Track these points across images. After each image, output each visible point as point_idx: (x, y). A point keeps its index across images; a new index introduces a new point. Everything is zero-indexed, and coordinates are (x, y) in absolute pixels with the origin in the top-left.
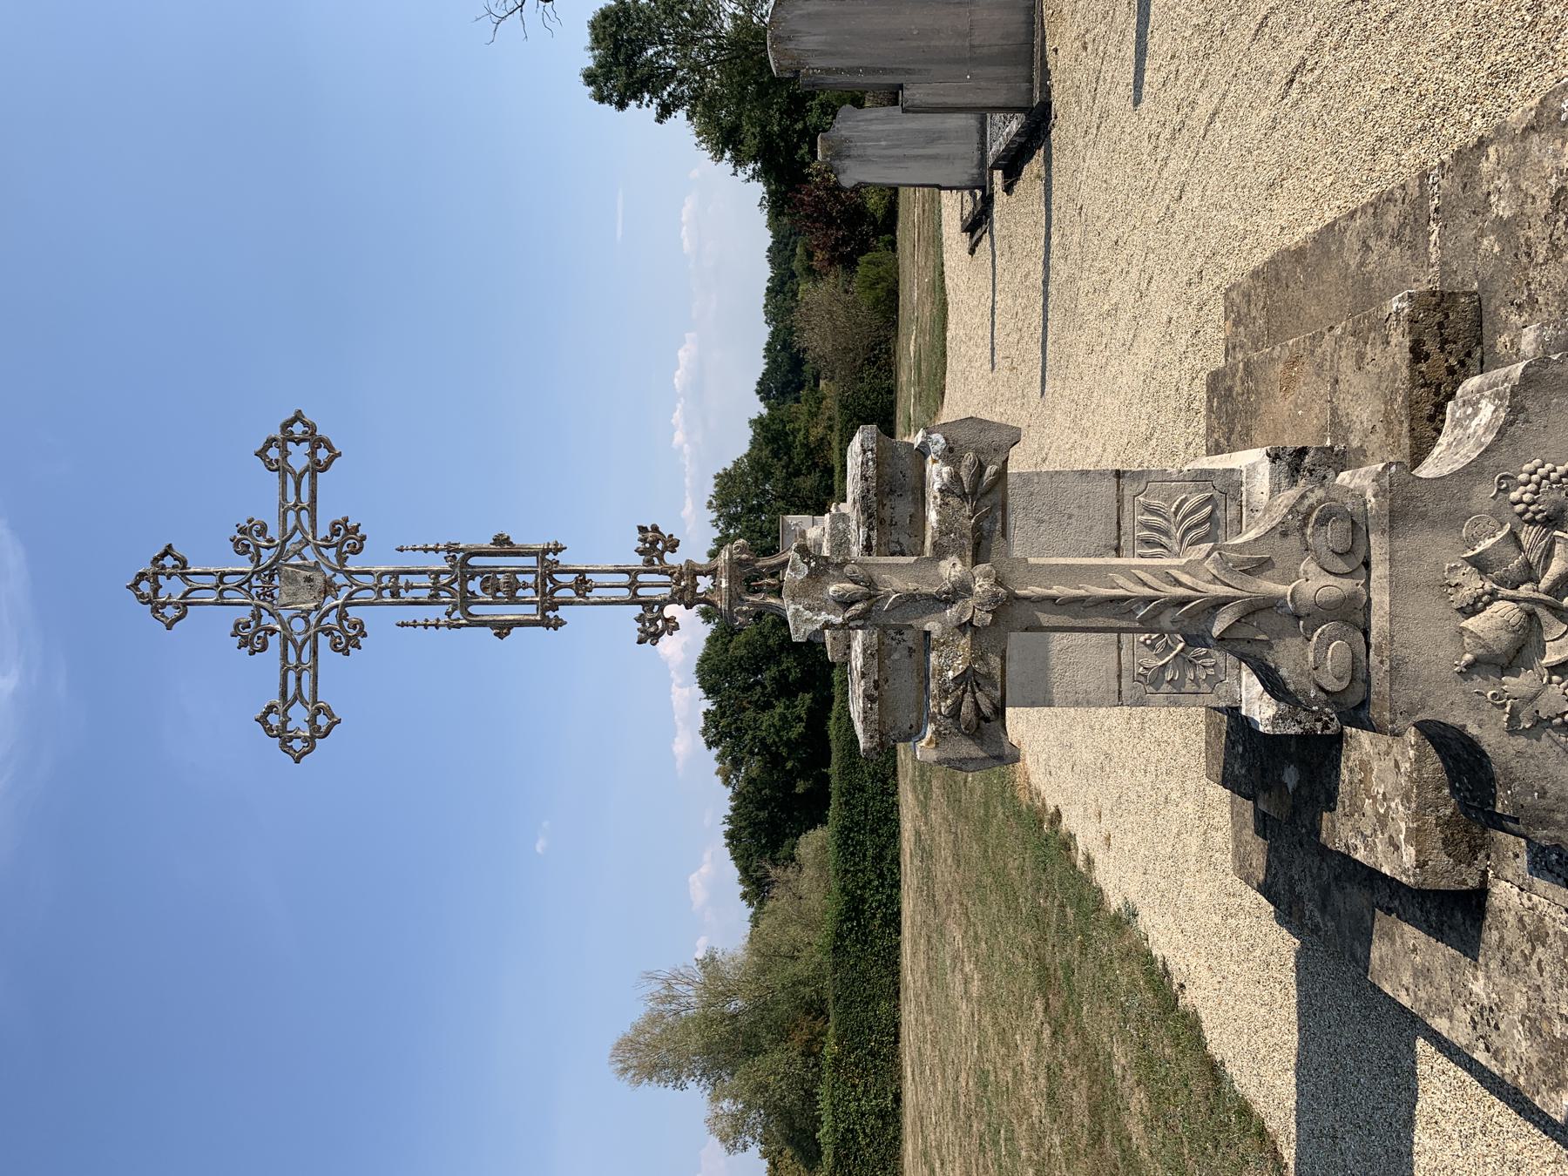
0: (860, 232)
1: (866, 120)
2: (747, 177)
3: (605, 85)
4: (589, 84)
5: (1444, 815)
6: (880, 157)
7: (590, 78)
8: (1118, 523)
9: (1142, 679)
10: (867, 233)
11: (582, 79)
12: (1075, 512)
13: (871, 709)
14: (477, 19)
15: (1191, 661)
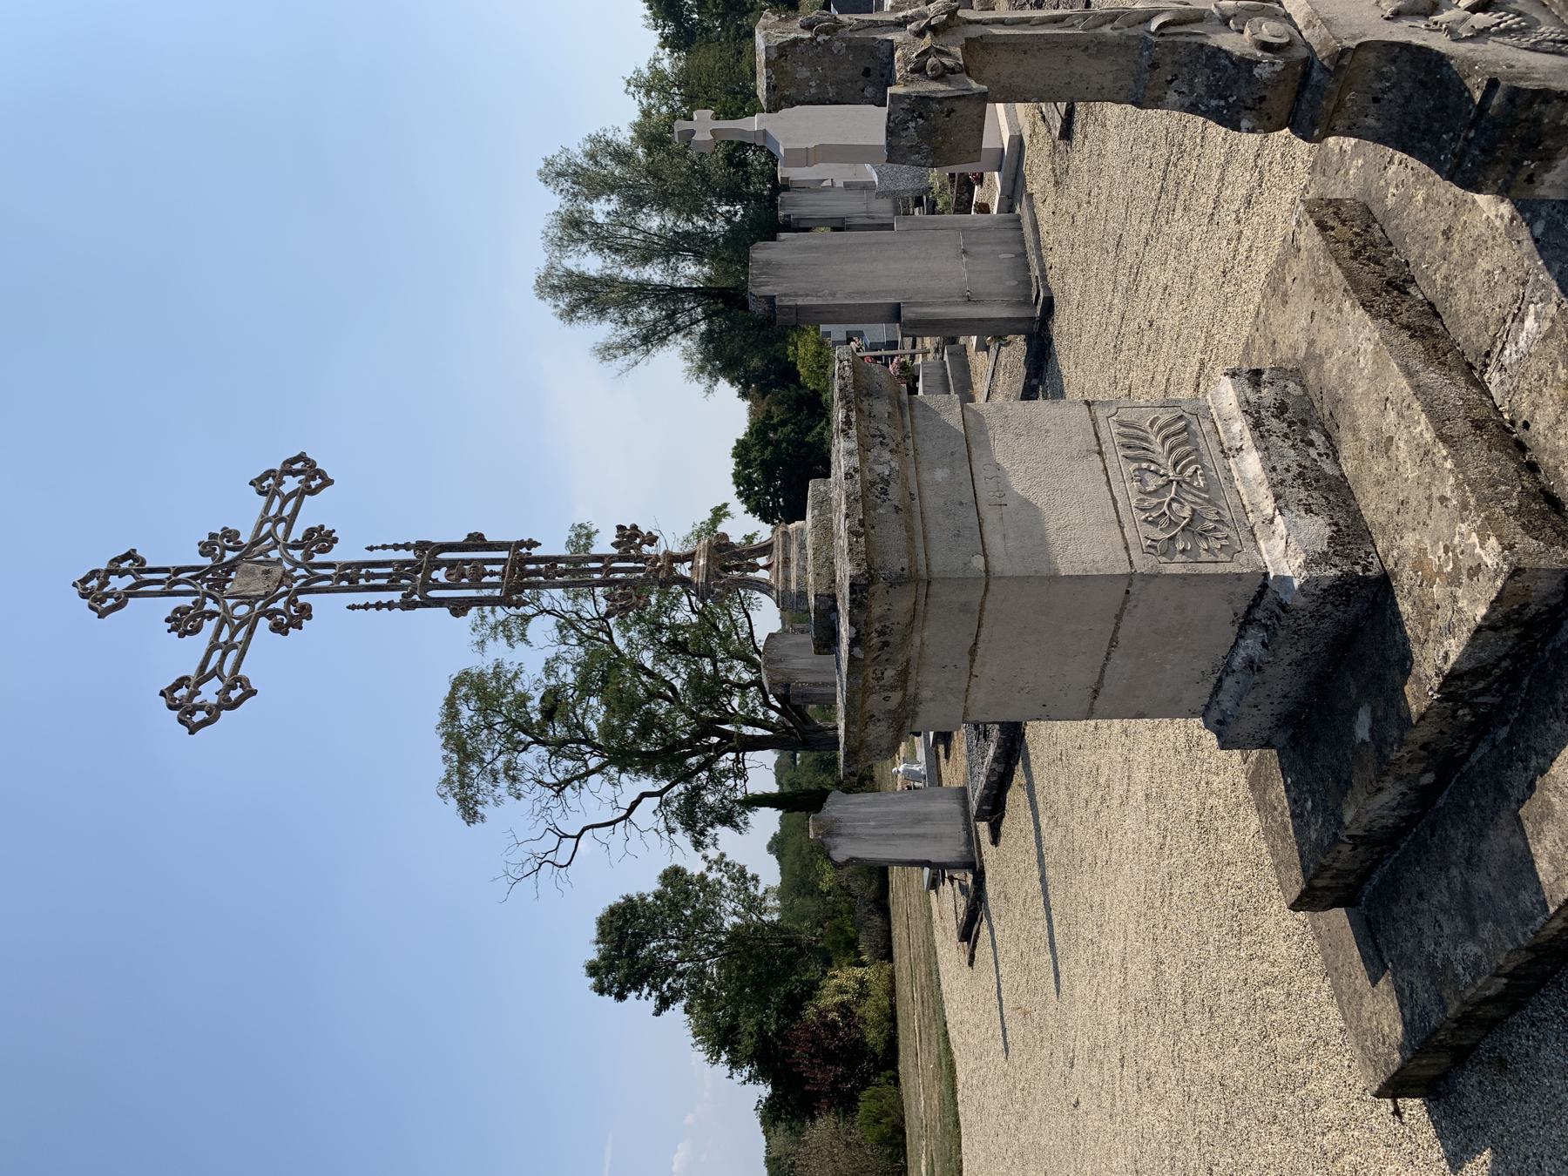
0: (860, 1070)
1: (855, 804)
2: (743, 1079)
3: (606, 977)
4: (591, 975)
6: (870, 835)
7: (593, 970)
8: (1096, 434)
9: (1152, 551)
10: (868, 1071)
11: (584, 970)
12: (1053, 428)
13: (857, 542)
14: (495, 879)
15: (1201, 535)
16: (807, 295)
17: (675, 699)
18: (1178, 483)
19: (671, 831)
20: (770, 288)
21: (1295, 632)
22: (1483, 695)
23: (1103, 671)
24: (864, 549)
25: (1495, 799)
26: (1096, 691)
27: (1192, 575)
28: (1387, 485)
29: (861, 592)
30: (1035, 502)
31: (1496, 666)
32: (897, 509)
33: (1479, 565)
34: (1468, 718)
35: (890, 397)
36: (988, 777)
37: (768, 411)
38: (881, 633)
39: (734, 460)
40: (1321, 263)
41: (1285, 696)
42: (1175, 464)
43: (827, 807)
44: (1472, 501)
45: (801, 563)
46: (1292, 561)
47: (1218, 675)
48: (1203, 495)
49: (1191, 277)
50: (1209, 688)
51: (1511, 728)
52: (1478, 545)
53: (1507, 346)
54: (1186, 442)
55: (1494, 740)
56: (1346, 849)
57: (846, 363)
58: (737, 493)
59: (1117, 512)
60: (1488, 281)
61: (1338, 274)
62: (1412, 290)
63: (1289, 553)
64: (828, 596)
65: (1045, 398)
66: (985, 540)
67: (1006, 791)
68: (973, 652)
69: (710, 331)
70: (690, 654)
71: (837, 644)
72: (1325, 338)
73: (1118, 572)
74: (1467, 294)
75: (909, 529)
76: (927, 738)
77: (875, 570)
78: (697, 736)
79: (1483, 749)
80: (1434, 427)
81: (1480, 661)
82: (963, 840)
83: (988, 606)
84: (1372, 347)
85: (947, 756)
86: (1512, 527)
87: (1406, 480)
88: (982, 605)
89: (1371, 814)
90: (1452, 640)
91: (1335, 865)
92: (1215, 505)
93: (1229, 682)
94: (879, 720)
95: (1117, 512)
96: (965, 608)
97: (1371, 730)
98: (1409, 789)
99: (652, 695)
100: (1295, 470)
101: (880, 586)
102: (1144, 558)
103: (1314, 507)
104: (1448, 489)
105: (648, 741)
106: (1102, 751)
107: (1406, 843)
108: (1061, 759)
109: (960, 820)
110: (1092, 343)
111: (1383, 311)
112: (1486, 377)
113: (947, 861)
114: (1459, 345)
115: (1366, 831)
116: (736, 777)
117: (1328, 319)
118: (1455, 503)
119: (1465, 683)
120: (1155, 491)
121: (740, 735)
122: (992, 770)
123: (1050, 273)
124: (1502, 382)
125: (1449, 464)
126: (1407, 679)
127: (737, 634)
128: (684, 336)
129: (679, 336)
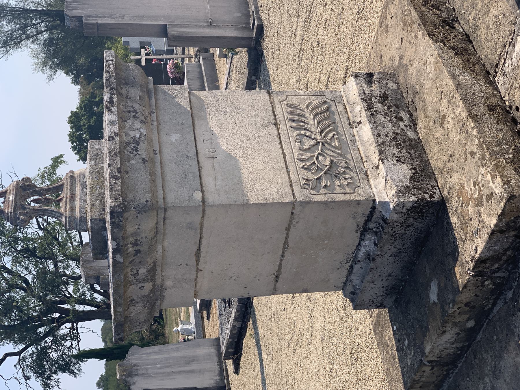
1: (147, 353)
5: (509, 158)
6: (157, 374)
8: (274, 112)
9: (307, 187)
12: (247, 108)
13: (115, 183)
15: (336, 176)
16: (105, 17)
17: (27, 287)
18: (323, 143)
19: (27, 378)
20: (79, 11)
21: (392, 236)
22: (498, 272)
23: (280, 264)
24: (120, 188)
25: (507, 335)
26: (277, 277)
27: (331, 202)
28: (443, 145)
29: (118, 217)
30: (235, 156)
31: (504, 254)
32: (144, 161)
33: (492, 193)
34: (491, 286)
35: (141, 86)
36: (231, 331)
37: (93, 93)
38: (134, 244)
39: (69, 125)
40: (406, 8)
41: (389, 276)
42: (321, 132)
43: (128, 357)
44: (488, 155)
45: (83, 198)
46: (389, 192)
47: (350, 264)
48: (337, 151)
49: (340, 15)
50: (345, 272)
51: (514, 291)
52: (491, 181)
53: (507, 61)
54: (328, 118)
55: (505, 298)
56: (427, 369)
57: (110, 62)
58: (72, 147)
59: (286, 162)
60: (496, 22)
61: (415, 14)
62: (457, 26)
63: (388, 187)
64: (100, 220)
65: (260, 88)
66: (203, 181)
67: (242, 339)
68: (198, 255)
69: (50, 39)
70: (38, 257)
71: (108, 252)
72: (409, 54)
73: (285, 201)
74: (486, 29)
75: (152, 174)
76: (195, 307)
77: (128, 202)
78: (43, 313)
79: (500, 304)
80: (467, 109)
81: (494, 251)
82: (217, 372)
83: (206, 224)
84: (433, 60)
85: (208, 318)
86: (509, 169)
87: (453, 141)
88: (202, 224)
89: (440, 347)
90: (479, 239)
91: (423, 379)
92: (345, 158)
93: (356, 268)
94: (137, 303)
95: (286, 162)
96: (190, 226)
97: (438, 295)
98: (461, 331)
99: (11, 287)
100: (391, 135)
101: (132, 212)
102: (302, 192)
103: (402, 159)
104: (475, 147)
105: (9, 318)
106: (297, 311)
107: (461, 364)
108: (274, 317)
109: (216, 359)
110: (286, 54)
111: (440, 38)
112: (496, 80)
113: (208, 386)
114: (482, 60)
115: (438, 358)
116: (72, 339)
117: (410, 42)
118: (479, 156)
119: (488, 265)
120: (309, 149)
121: (75, 311)
122: (234, 326)
123: (261, 10)
124: (504, 83)
125: (475, 132)
126: (456, 264)
127: (71, 243)
128: (33, 42)
129: (29, 42)
